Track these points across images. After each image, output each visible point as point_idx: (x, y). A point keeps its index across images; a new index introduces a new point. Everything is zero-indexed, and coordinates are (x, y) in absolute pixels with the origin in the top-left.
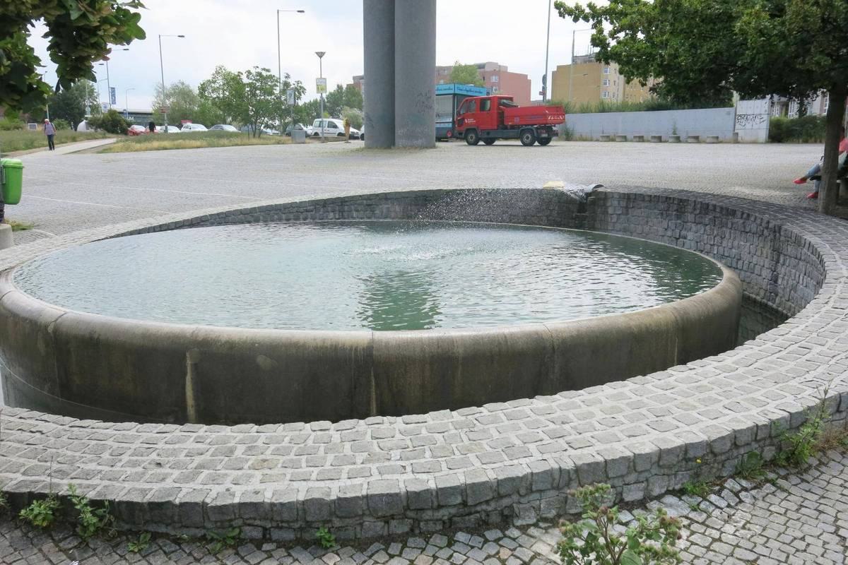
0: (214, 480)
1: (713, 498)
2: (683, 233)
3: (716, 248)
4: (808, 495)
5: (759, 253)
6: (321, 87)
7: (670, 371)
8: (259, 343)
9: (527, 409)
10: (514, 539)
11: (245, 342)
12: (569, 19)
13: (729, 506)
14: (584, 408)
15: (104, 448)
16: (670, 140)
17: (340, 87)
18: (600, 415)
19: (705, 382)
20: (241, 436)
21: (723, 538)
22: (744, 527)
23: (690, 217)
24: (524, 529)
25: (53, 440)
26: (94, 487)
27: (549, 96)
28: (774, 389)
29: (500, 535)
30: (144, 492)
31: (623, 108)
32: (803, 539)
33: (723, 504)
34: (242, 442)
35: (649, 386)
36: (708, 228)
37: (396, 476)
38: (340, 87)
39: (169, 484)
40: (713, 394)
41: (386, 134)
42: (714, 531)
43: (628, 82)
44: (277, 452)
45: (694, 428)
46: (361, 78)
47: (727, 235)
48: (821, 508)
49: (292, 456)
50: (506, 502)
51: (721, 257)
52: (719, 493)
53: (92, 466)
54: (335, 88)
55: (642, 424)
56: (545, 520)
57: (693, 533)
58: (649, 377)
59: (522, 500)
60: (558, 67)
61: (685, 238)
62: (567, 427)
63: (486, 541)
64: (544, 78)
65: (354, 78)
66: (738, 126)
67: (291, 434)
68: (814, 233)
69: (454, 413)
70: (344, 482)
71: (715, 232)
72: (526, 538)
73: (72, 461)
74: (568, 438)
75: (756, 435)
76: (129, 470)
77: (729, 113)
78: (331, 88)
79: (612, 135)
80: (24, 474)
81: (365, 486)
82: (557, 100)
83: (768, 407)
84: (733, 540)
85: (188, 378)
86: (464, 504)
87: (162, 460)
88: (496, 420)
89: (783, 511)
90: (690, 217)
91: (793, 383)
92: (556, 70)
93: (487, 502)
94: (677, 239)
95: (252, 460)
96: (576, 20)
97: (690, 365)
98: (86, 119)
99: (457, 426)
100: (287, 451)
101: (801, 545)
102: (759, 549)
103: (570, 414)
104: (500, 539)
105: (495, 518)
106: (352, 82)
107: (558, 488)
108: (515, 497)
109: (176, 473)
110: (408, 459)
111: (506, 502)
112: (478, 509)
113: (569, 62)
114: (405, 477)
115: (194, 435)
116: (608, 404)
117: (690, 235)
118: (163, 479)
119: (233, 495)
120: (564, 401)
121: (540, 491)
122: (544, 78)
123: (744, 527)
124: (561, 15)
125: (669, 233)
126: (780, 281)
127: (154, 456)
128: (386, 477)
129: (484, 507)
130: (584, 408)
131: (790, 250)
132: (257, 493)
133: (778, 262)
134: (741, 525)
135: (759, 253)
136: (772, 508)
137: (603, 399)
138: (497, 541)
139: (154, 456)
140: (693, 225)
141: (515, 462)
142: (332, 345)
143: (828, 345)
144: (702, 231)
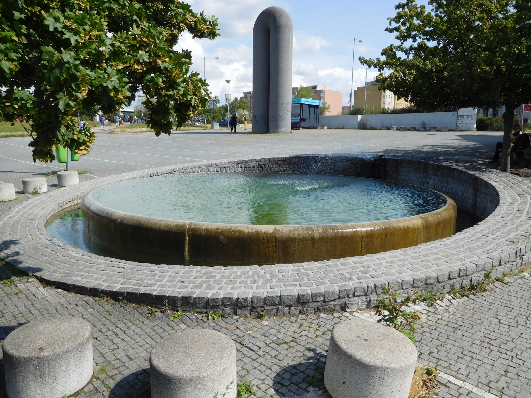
0: (211, 288)
1: (438, 302)
2: (427, 180)
3: (444, 188)
4: (484, 302)
5: (467, 191)
6: (227, 100)
7: (419, 246)
8: (221, 230)
9: (351, 262)
10: (347, 317)
11: (154, 227)
12: (366, 66)
13: (446, 306)
14: (378, 261)
15: (155, 275)
16: (421, 129)
17: (236, 99)
18: (385, 264)
19: (436, 251)
20: (218, 271)
21: (443, 319)
22: (453, 315)
23: (431, 172)
24: (351, 313)
25: (130, 271)
26: (156, 290)
27: (353, 104)
28: (468, 254)
29: (341, 315)
30: (179, 293)
31: (395, 112)
32: (481, 319)
33: (443, 305)
34: (219, 273)
35: (408, 252)
36: (440, 178)
37: (293, 288)
38: (236, 99)
39: (189, 289)
40: (439, 256)
41: (265, 124)
42: (439, 316)
43: (398, 99)
44: (237, 277)
45: (430, 270)
46: (249, 93)
47: (450, 181)
48: (490, 307)
49: (243, 279)
50: (343, 301)
51: (447, 194)
52: (442, 300)
53: (152, 282)
54: (233, 99)
55: (405, 268)
56: (360, 309)
57: (429, 316)
58: (408, 248)
59: (350, 300)
60: (358, 88)
61: (428, 183)
62: (370, 269)
63: (334, 317)
64: (351, 94)
65: (244, 93)
66: (459, 122)
67: (241, 270)
68: (495, 181)
69: (316, 263)
70: (269, 289)
71: (444, 180)
72: (352, 316)
73: (142, 280)
74: (370, 273)
75: (459, 274)
76: (170, 284)
77: (453, 115)
78: (232, 99)
79: (389, 126)
80: (121, 284)
81: (279, 292)
82: (358, 107)
83: (465, 262)
84: (448, 320)
85: (186, 246)
86: (324, 301)
87: (183, 280)
88: (336, 265)
89: (472, 308)
90: (431, 172)
91: (478, 251)
92: (356, 89)
93: (334, 300)
94: (424, 184)
95: (225, 281)
96: (370, 66)
97: (429, 243)
98: (99, 115)
99: (319, 268)
100: (240, 277)
101: (479, 322)
102: (460, 323)
103: (371, 264)
104: (340, 317)
105: (338, 308)
106: (243, 96)
107: (366, 295)
108: (347, 298)
109: (191, 285)
110: (297, 281)
111: (343, 301)
112: (331, 303)
113: (363, 85)
114: (296, 288)
115: (195, 270)
116: (389, 260)
117: (431, 182)
118: (186, 288)
119: (220, 294)
120: (433, 245)
121: (358, 296)
122: (351, 94)
123: (453, 315)
124: (362, 63)
125: (420, 180)
126: (477, 206)
127: (179, 278)
128: (288, 288)
129: (333, 302)
130: (378, 261)
131: (483, 189)
132: (230, 293)
133: (476, 195)
134: (452, 313)
135: (467, 191)
136: (467, 307)
137: (387, 258)
138: (339, 317)
139: (179, 278)
140: (432, 177)
141: (347, 283)
142: (265, 232)
143: (497, 235)
144: (437, 180)
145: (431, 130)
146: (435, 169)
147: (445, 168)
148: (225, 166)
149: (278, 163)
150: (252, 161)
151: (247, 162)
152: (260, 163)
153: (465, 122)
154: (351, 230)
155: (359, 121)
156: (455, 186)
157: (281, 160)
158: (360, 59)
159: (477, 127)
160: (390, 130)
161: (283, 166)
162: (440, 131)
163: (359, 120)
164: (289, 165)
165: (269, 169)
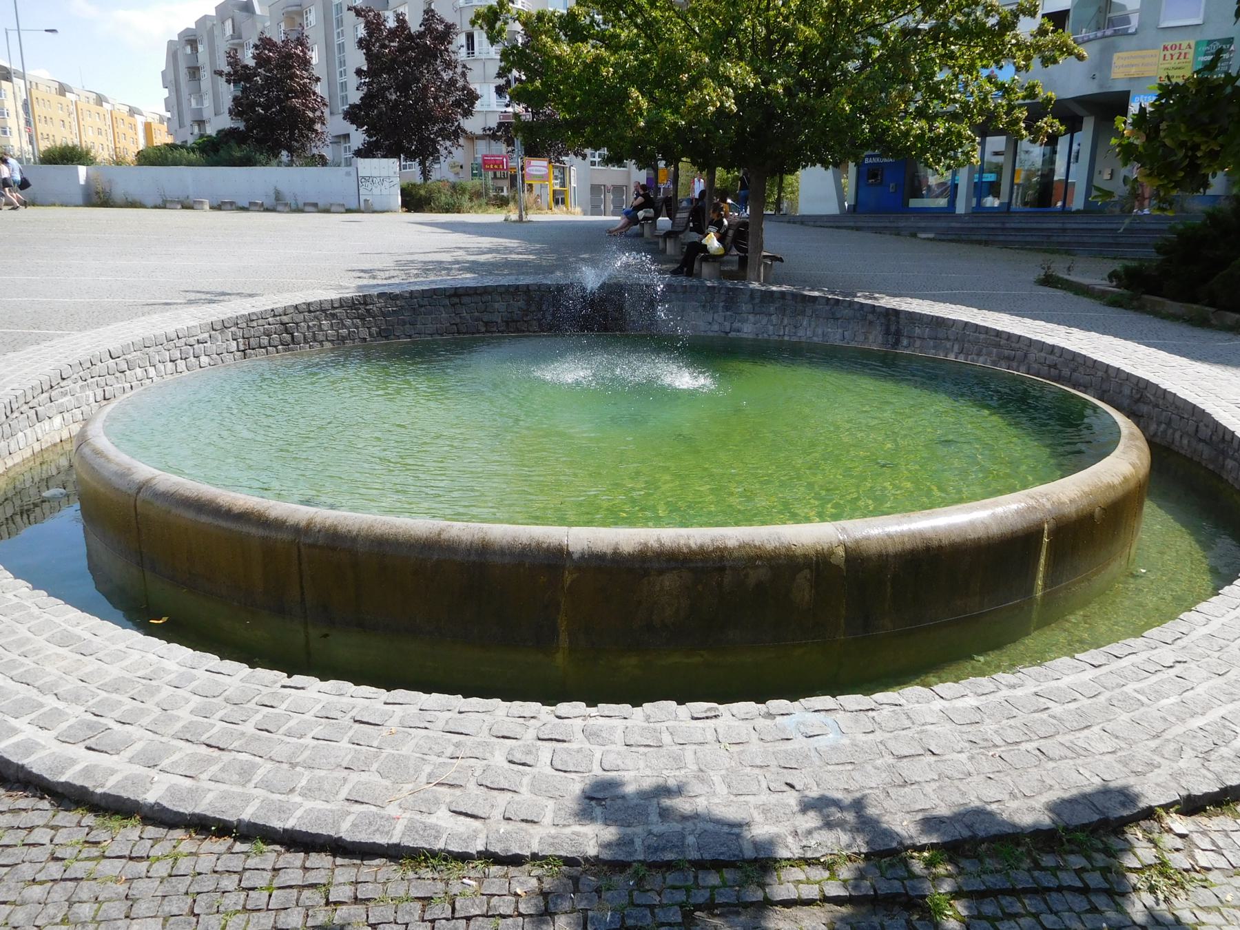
2: (737, 325)
36: (774, 317)
71: (786, 321)
77: (348, 174)
144: (764, 321)
145: (307, 209)
146: (757, 301)
147: (789, 297)
148: (192, 340)
149: (334, 316)
150: (262, 316)
151: (249, 319)
152: (285, 319)
153: (376, 191)
154: (175, 478)
155: (82, 182)
156: (820, 332)
157: (341, 306)
158: (1230, 41)
159: (403, 205)
160: (191, 208)
161: (348, 322)
162: (327, 211)
163: (82, 181)
164: (363, 319)
165: (309, 335)
